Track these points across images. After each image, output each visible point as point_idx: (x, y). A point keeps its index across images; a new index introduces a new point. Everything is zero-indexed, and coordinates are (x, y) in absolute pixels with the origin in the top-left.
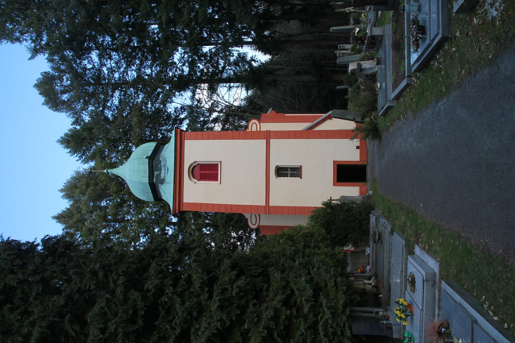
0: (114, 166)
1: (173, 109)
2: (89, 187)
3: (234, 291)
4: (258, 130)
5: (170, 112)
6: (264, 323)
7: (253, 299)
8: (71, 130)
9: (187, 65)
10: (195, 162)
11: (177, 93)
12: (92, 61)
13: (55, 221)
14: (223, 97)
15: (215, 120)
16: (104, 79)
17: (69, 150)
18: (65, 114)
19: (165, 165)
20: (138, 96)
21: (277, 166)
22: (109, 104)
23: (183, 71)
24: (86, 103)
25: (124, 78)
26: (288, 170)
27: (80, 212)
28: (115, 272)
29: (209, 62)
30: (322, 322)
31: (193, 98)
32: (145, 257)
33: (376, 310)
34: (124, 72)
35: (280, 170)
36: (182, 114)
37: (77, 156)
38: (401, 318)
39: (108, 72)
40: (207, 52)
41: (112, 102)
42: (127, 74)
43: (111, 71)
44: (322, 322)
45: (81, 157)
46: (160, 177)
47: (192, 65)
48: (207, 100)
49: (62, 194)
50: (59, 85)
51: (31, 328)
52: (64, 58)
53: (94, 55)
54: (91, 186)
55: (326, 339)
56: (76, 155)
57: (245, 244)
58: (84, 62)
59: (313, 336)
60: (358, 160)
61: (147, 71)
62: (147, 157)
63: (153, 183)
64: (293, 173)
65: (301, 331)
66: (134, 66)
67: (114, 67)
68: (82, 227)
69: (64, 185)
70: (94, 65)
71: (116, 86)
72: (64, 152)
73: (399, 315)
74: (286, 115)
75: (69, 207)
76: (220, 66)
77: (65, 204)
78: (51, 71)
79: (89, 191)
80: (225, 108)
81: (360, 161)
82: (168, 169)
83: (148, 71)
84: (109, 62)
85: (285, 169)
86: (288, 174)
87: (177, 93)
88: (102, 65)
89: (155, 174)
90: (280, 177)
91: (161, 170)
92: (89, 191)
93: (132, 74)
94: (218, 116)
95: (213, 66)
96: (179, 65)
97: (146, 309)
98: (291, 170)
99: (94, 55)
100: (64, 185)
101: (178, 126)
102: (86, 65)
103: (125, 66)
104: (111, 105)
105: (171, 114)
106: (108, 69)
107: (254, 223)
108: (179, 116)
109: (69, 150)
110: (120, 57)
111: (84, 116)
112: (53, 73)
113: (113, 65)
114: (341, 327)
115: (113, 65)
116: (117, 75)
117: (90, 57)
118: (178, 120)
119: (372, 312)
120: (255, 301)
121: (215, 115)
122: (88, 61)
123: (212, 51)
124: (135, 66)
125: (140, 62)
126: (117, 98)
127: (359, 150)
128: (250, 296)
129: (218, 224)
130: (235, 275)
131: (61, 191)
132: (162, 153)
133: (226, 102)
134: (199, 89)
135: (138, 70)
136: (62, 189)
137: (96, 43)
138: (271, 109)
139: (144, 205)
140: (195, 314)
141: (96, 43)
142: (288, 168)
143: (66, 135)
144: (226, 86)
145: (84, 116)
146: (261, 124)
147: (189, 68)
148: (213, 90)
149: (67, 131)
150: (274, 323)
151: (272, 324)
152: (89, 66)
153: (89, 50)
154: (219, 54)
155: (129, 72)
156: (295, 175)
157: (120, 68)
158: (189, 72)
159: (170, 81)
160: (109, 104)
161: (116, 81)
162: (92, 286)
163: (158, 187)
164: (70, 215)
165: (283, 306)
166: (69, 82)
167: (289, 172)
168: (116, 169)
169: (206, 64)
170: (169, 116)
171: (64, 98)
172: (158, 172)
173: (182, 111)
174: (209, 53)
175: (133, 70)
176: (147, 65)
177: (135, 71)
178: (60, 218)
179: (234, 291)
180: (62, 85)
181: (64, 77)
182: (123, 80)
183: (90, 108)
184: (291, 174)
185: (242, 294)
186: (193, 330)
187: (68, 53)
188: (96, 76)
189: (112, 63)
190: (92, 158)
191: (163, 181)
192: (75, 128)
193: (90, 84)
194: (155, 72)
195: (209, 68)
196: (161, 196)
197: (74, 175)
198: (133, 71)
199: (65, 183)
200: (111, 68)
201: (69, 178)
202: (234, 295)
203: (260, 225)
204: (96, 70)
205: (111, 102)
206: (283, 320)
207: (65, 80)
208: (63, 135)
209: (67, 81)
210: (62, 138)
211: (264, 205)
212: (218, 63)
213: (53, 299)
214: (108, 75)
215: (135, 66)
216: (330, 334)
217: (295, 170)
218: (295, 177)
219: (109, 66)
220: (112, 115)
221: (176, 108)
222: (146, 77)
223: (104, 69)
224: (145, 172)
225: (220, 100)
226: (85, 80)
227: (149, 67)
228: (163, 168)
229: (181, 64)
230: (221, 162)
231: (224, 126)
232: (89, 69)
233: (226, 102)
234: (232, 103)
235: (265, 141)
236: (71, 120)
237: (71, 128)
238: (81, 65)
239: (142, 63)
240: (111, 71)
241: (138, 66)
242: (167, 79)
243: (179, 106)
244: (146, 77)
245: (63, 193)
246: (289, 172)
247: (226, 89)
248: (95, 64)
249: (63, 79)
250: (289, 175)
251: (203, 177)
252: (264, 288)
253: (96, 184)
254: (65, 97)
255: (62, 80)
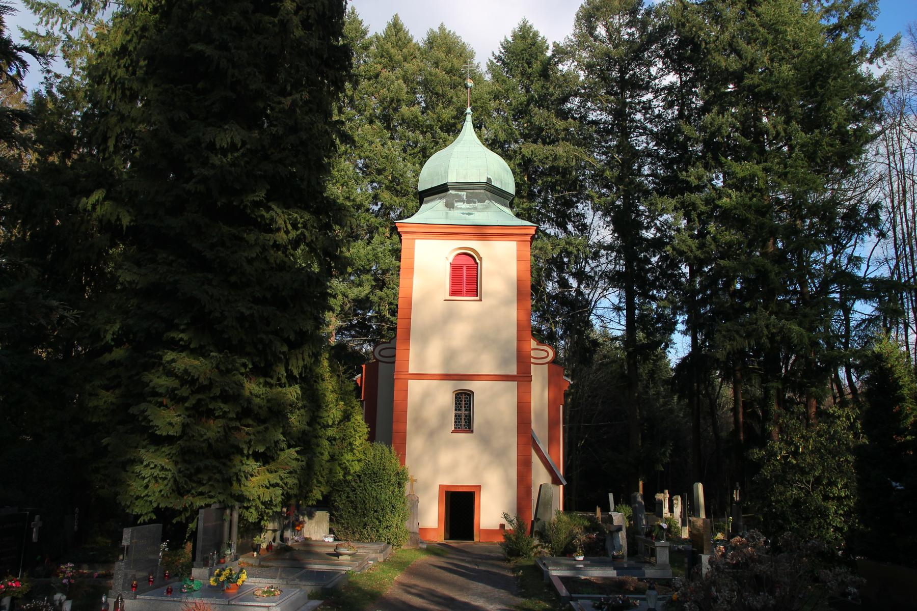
0: (478, 126)
1: (583, 212)
2: (447, 73)
3: (264, 337)
4: (533, 360)
5: (577, 207)
6: (218, 380)
7: (253, 364)
8: (544, 41)
9: (658, 235)
10: (480, 259)
11: (608, 219)
12: (662, 76)
13: (391, 21)
14: (604, 296)
15: (564, 284)
16: (631, 96)
17: (510, 39)
18: (572, 32)
19: (476, 209)
20: (603, 153)
21: (473, 393)
22: (589, 104)
23: (648, 228)
24: (590, 67)
25: (635, 129)
26: (466, 410)
27: (405, 60)
28: (295, 160)
29: (664, 273)
30: (218, 465)
31: (600, 245)
32: (318, 201)
33: (234, 545)
34: (645, 128)
35: (467, 398)
36: (574, 227)
37: (501, 52)
38: (219, 575)
39: (644, 102)
40: (680, 269)
41: (593, 110)
42: (641, 135)
43: (647, 107)
44: (218, 465)
45: (499, 59)
46: (457, 201)
47: (657, 245)
48: (597, 269)
49: (436, 30)
50: (621, 21)
51: (217, 43)
52: (664, 30)
53: (672, 78)
54: (450, 77)
55: (193, 471)
56: (503, 51)
57: (353, 333)
58: (661, 63)
59: (197, 451)
60: (416, 241)
61: (646, 167)
62: (489, 180)
63: (447, 190)
64: (461, 419)
65: (205, 434)
66: (654, 146)
67: (653, 111)
68: (380, 63)
69: (452, 32)
70: (655, 78)
71: (620, 114)
72: (506, 31)
73: (224, 573)
74: (561, 406)
75: (414, 41)
76: (655, 292)
77: (418, 35)
78: (644, 7)
79: (442, 74)
80: (584, 298)
81: (480, 530)
82: (469, 214)
83: (646, 170)
84: (661, 104)
85: (469, 406)
86: (459, 410)
87: (608, 219)
88: (657, 92)
89: (462, 193)
90: (456, 398)
91: (468, 202)
92: (442, 74)
93: (641, 142)
94: (572, 287)
95: (657, 279)
96: (658, 222)
97: (242, 207)
98: (466, 416)
99: (672, 78)
100: (452, 32)
101: (553, 221)
102: (656, 65)
103: (655, 130)
104: (589, 108)
105: (572, 207)
106: (650, 101)
107: (382, 353)
108: (570, 220)
109: (510, 39)
110: (670, 122)
111: (569, 63)
112: (642, 12)
113: (656, 111)
114: (210, 492)
115: (656, 111)
116: (639, 116)
117: (669, 72)
118: (564, 219)
119: (230, 538)
120: (250, 366)
121: (573, 283)
122: (662, 69)
123: (682, 277)
124: (655, 148)
125: (662, 156)
126: (599, 117)
127: (498, 528)
128: (257, 359)
129: (385, 289)
130: (289, 337)
131: (442, 28)
132: (496, 204)
133: (596, 302)
134: (616, 257)
135: (648, 153)
136: (445, 29)
137: (693, 82)
138: (572, 383)
139: (417, 165)
140: (233, 279)
141: (693, 82)
142: (470, 410)
143: (536, 34)
144: (620, 302)
145: (569, 63)
146: (547, 365)
147: (652, 238)
148: (615, 279)
149: (541, 35)
150: (218, 394)
151: (217, 391)
152: (654, 70)
153: (679, 71)
154: (676, 289)
155: (644, 137)
156: (459, 422)
157: (651, 122)
158: (646, 240)
159: (630, 207)
160: (589, 104)
161: (630, 116)
162: (275, 129)
163: (441, 198)
164: (400, 43)
165: (243, 407)
166: (626, 37)
167: (463, 412)
168: (472, 127)
169: (660, 267)
170: (571, 204)
171: (598, 29)
172: (465, 197)
173: (579, 226)
174: (679, 273)
175: (648, 144)
176: (656, 169)
177: (646, 147)
178: (396, 27)
179: (264, 337)
180: (621, 26)
181: (633, 29)
182: (630, 128)
183: (581, 73)
184: (459, 416)
185: (260, 347)
186: (210, 276)
187: (673, 39)
188: (637, 82)
189: (660, 108)
190: (496, 77)
191: (450, 206)
192: (547, 48)
193: (623, 72)
194: (645, 182)
195: (653, 273)
196: (427, 202)
197: (469, 49)
198: (645, 145)
199: (454, 33)
200: (650, 108)
201: (463, 41)
202: (259, 336)
203: (380, 363)
204: (648, 82)
205: (593, 107)
206: (222, 407)
207: (629, 31)
208: (535, 28)
209: (628, 34)
210: (531, 27)
211: (410, 372)
212: (661, 287)
213: (257, 74)
214: (639, 102)
215: (655, 148)
216: (200, 476)
217: (466, 422)
218: (455, 422)
219: (655, 103)
220: (570, 110)
221: (583, 216)
222: (636, 167)
223: (650, 96)
224: (465, 178)
225: (599, 290)
226: (629, 64)
227: (653, 170)
228: (472, 205)
229: (658, 225)
230: (481, 300)
231: (554, 297)
232: (648, 71)
233: (596, 302)
234: (594, 311)
235: (515, 373)
236: (562, 42)
237: (547, 42)
238: (655, 58)
239: (659, 158)
240: (647, 107)
241: (654, 152)
242: (634, 202)
243: (588, 221)
244: (636, 167)
245: (438, 31)
246: (463, 412)
247: (616, 301)
248: (657, 81)
249: (631, 28)
250: (459, 412)
251: (456, 271)
252: (269, 380)
253: (454, 87)
254: (601, 31)
255: (630, 24)
